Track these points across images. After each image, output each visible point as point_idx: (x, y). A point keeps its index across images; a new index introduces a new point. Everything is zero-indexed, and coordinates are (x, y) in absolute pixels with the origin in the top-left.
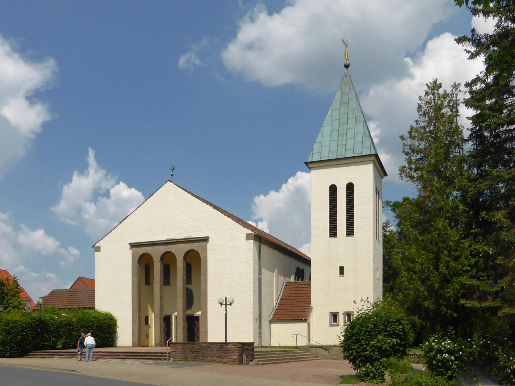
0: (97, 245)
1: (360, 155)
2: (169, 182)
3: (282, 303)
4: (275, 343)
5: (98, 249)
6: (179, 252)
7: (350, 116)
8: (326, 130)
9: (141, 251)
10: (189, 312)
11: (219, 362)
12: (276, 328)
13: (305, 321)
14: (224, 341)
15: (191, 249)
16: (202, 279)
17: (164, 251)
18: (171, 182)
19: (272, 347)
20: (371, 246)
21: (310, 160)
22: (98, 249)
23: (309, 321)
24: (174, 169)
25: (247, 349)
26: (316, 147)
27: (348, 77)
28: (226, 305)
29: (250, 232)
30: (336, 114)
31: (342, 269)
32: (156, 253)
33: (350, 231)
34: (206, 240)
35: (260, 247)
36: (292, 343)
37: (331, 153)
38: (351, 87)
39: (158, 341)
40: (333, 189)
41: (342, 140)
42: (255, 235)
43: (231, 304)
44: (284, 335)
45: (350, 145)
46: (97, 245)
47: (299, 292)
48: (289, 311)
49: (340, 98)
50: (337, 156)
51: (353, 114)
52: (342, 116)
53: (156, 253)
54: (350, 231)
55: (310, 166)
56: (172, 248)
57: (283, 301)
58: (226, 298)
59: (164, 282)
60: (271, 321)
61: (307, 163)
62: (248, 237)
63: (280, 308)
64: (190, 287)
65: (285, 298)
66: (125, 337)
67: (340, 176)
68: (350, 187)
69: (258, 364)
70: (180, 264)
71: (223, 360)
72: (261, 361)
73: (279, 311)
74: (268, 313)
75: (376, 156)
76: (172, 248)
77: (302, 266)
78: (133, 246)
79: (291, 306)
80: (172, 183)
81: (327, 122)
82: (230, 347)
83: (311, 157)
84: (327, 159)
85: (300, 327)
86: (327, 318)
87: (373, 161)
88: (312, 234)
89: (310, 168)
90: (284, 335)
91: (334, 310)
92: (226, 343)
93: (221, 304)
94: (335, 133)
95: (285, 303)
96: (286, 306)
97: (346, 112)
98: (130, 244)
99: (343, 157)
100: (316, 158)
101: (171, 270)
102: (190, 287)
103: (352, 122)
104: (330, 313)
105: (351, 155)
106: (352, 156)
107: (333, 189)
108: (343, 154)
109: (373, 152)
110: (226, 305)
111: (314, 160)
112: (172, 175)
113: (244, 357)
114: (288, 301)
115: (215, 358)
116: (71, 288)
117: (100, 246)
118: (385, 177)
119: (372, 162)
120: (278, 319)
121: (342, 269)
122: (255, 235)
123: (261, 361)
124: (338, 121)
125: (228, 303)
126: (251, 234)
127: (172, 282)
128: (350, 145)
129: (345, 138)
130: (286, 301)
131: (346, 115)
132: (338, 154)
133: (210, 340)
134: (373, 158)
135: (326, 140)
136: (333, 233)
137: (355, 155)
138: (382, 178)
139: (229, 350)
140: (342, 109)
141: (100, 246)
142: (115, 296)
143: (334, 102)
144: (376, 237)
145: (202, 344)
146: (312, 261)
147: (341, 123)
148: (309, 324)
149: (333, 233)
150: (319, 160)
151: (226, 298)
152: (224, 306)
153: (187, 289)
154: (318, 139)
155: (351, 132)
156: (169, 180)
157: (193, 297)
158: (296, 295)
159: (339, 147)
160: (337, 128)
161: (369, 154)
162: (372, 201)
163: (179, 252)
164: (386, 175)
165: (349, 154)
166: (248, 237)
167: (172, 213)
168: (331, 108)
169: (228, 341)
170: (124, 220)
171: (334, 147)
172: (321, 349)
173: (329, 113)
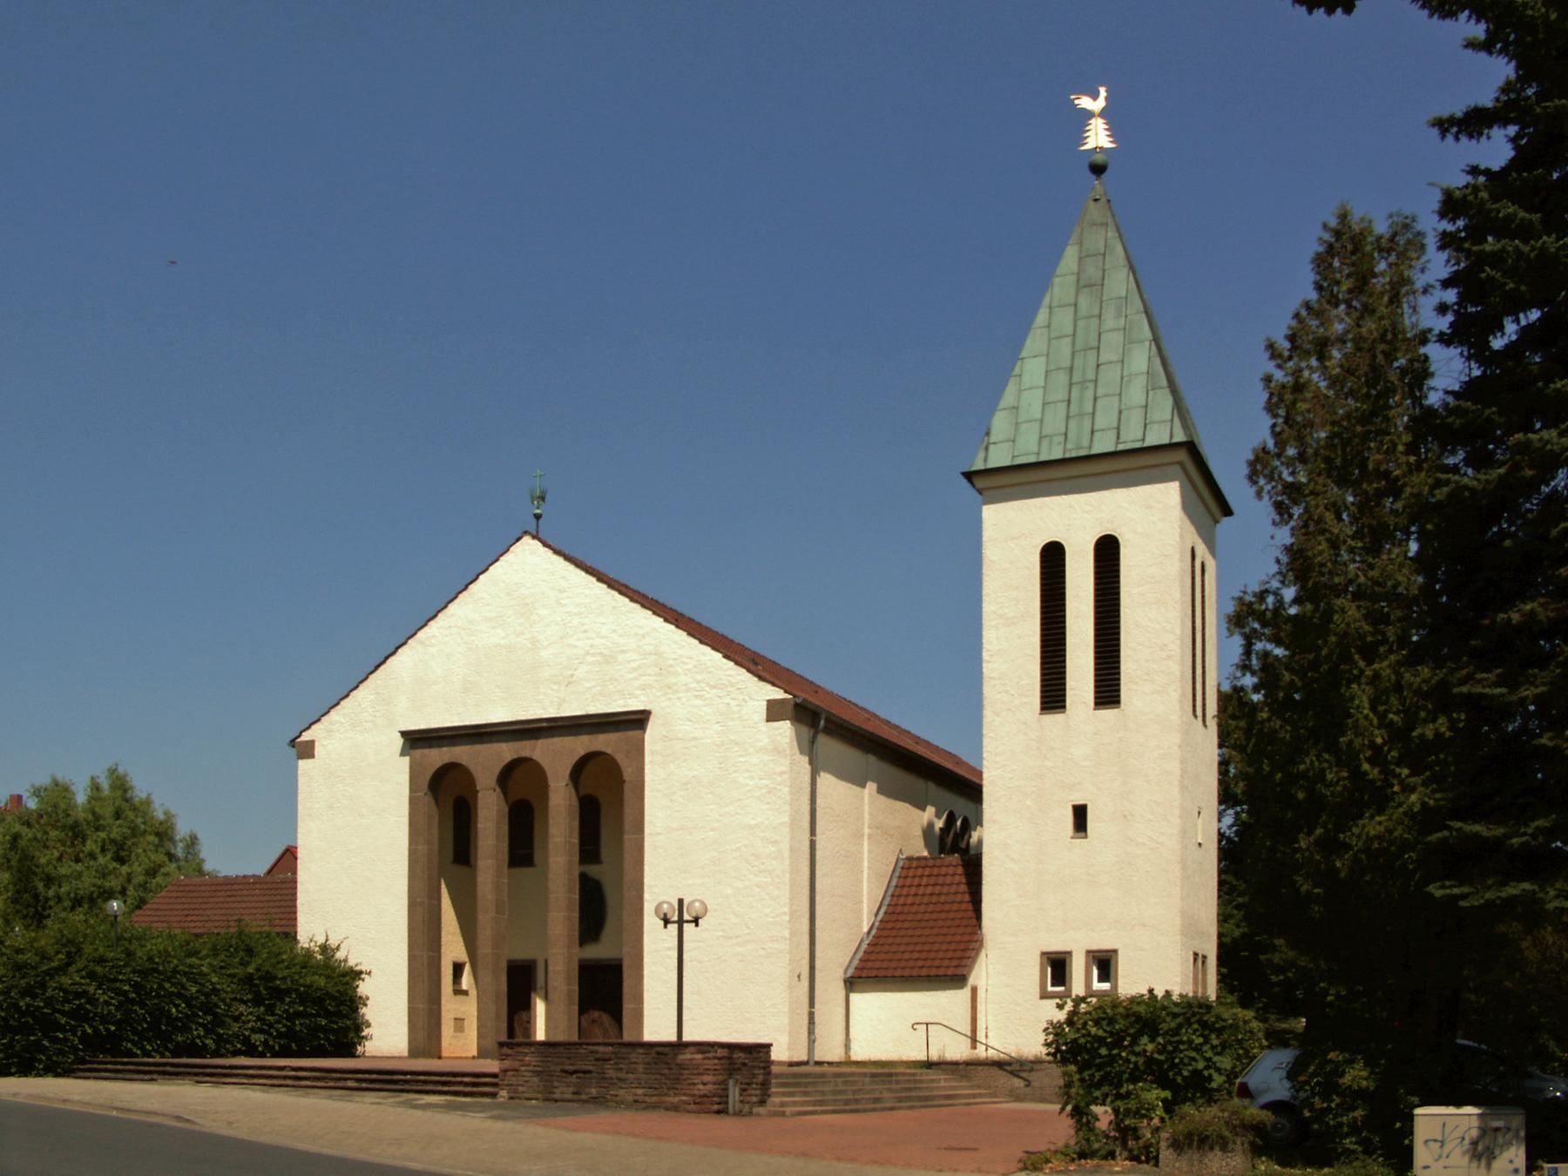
0: (306, 737)
1: (1138, 445)
2: (527, 540)
3: (890, 925)
4: (860, 1052)
5: (307, 751)
6: (556, 758)
7: (1109, 323)
8: (1032, 369)
9: (438, 756)
10: (595, 952)
11: (654, 1107)
12: (867, 1004)
13: (957, 979)
14: (673, 1038)
15: (593, 748)
16: (627, 844)
17: (446, 760)
18: (534, 537)
19: (857, 1063)
20: (1175, 739)
21: (979, 465)
22: (307, 751)
23: (971, 981)
24: (543, 498)
25: (744, 1064)
26: (1000, 424)
27: (1103, 200)
28: (681, 922)
29: (778, 694)
30: (1064, 320)
31: (1080, 813)
32: (485, 762)
33: (1108, 692)
34: (637, 720)
35: (813, 742)
36: (912, 1049)
37: (1045, 443)
38: (1112, 234)
39: (490, 1043)
40: (1053, 557)
41: (1081, 398)
42: (797, 706)
43: (696, 921)
44: (889, 1026)
45: (1105, 419)
46: (306, 737)
47: (945, 889)
48: (910, 948)
49: (1075, 269)
50: (1065, 451)
51: (1118, 316)
52: (1081, 324)
53: (485, 762)
54: (1108, 692)
55: (980, 483)
56: (538, 750)
57: (894, 917)
58: (681, 902)
59: (581, 852)
60: (855, 982)
61: (969, 476)
62: (774, 712)
63: (882, 941)
64: (593, 870)
65: (899, 909)
66: (387, 1030)
67: (1077, 519)
68: (1107, 551)
69: (783, 1114)
70: (561, 802)
71: (667, 1099)
72: (795, 1104)
73: (878, 949)
74: (837, 956)
75: (1191, 447)
76: (538, 750)
77: (961, 806)
78: (415, 740)
79: (918, 932)
80: (536, 542)
81: (1035, 342)
82: (689, 1056)
83: (981, 455)
84: (1032, 459)
85: (946, 1004)
86: (1032, 972)
87: (1181, 464)
88: (986, 702)
89: (980, 492)
90: (889, 1026)
91: (1056, 945)
92: (680, 1045)
93: (666, 922)
94: (1061, 378)
95: (899, 925)
96: (902, 933)
97: (1096, 312)
98: (404, 734)
99: (1083, 453)
100: (999, 457)
101: (534, 818)
102: (593, 870)
103: (1113, 341)
104: (1043, 954)
105: (1110, 448)
106: (1112, 449)
107: (1053, 557)
108: (1086, 443)
109: (1180, 437)
110: (681, 922)
111: (992, 464)
112: (538, 517)
113: (734, 1093)
114: (910, 917)
115: (640, 1091)
116: (269, 872)
117: (313, 742)
118: (1226, 520)
119: (1177, 468)
120: (874, 973)
121: (1080, 813)
122: (797, 706)
123: (795, 1104)
124: (1068, 340)
125: (686, 917)
126: (782, 701)
127: (605, 852)
128: (1105, 419)
129: (1089, 394)
130: (901, 917)
131: (1095, 321)
132: (1069, 446)
133: (649, 1035)
134: (1182, 455)
135: (1032, 403)
136: (1053, 696)
137: (1121, 447)
138: (1216, 521)
139: (681, 1067)
140: (1084, 302)
141: (313, 742)
142: (356, 894)
143: (1056, 280)
144: (1196, 707)
145: (601, 1049)
146: (985, 790)
147: (1079, 345)
148: (974, 990)
149: (1053, 696)
150: (1007, 463)
151: (681, 902)
152: (673, 928)
153: (585, 879)
154: (1008, 398)
155: (1110, 376)
156: (526, 533)
157: (602, 904)
158: (935, 899)
159: (1073, 425)
160: (1067, 364)
161: (1166, 441)
162: (1177, 595)
163: (556, 758)
164: (1227, 511)
165: (1104, 444)
166: (774, 712)
167: (531, 635)
168: (1046, 301)
169: (686, 1038)
170: (387, 658)
171: (1055, 423)
172: (996, 1071)
173: (1042, 317)
